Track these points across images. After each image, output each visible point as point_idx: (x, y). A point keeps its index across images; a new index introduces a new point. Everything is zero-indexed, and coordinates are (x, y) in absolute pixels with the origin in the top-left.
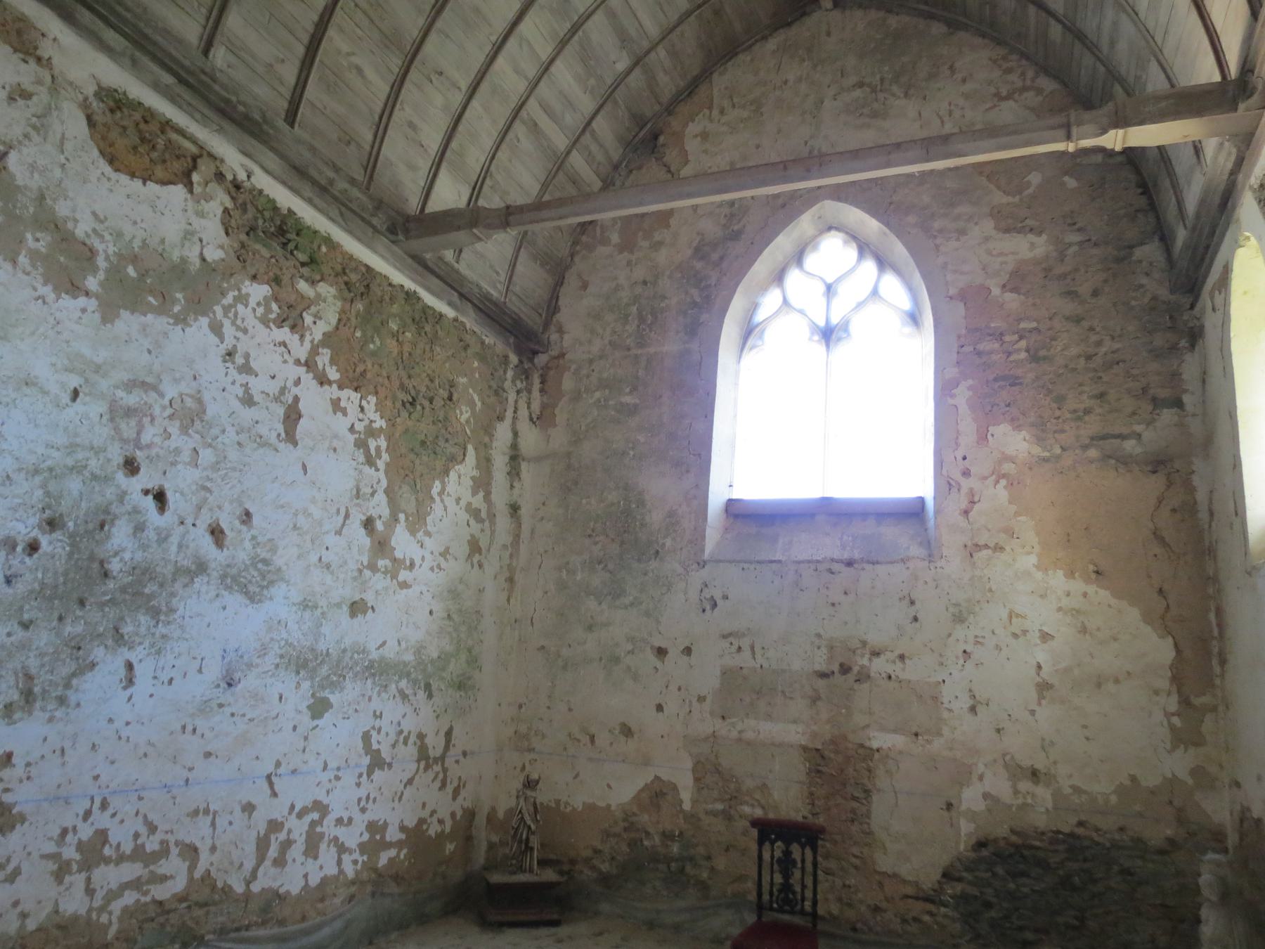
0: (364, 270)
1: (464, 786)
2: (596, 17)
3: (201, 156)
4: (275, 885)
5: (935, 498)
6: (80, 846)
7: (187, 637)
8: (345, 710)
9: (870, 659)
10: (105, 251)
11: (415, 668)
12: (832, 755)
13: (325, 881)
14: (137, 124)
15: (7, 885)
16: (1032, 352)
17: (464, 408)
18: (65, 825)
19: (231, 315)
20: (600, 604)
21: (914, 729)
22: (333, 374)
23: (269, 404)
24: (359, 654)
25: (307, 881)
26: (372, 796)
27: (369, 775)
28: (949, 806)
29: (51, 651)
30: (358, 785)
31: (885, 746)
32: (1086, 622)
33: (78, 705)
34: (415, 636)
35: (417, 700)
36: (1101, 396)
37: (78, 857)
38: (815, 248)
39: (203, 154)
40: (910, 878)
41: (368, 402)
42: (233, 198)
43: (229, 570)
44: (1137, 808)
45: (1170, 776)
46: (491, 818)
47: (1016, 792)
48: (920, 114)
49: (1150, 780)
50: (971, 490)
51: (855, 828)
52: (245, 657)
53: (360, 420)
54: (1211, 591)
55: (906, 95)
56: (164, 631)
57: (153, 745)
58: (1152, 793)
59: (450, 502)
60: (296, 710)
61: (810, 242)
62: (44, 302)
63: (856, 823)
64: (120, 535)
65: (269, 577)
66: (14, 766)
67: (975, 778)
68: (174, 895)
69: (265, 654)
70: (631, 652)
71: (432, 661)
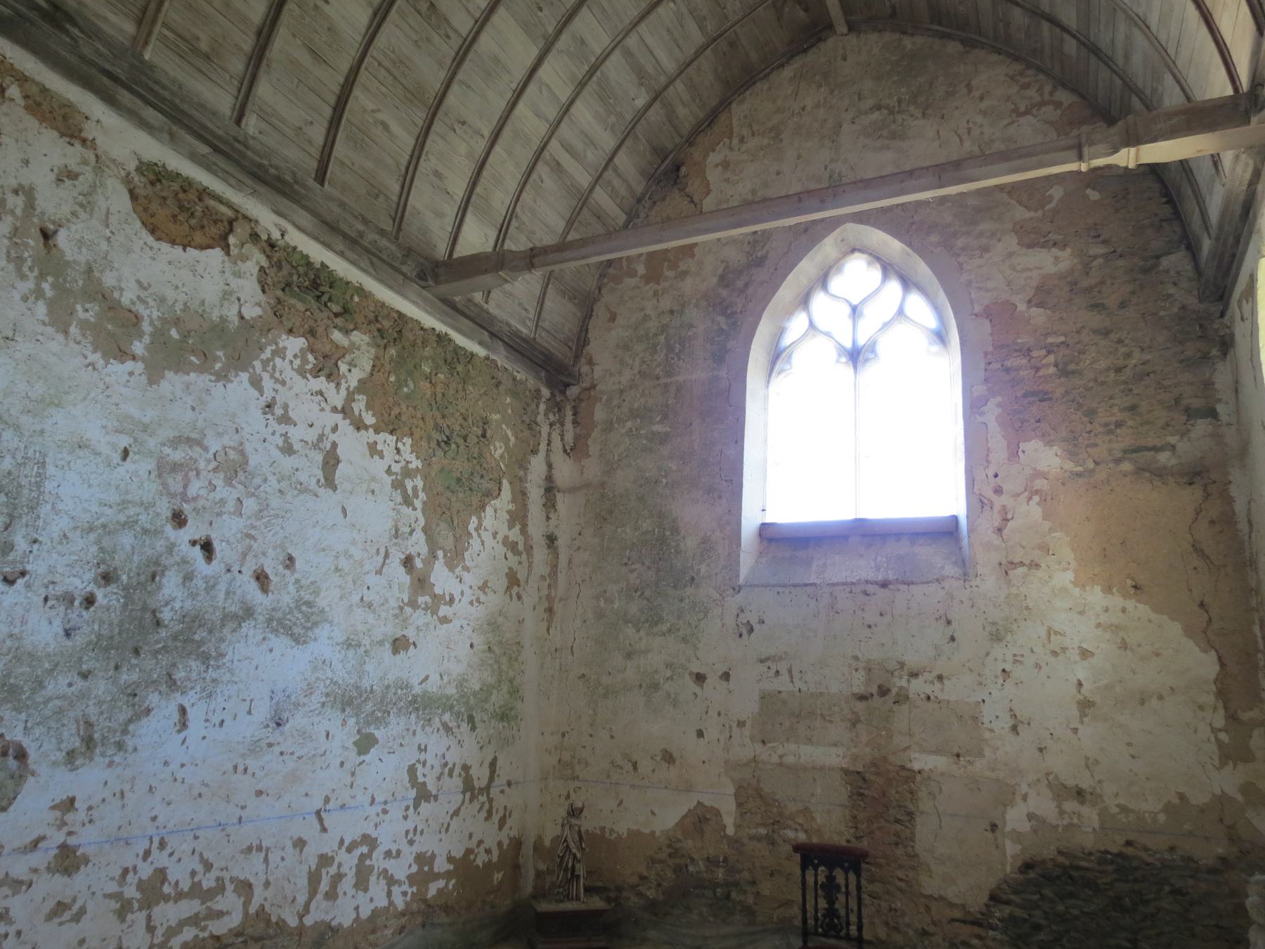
0: (396, 316)
1: (510, 816)
2: (613, 57)
3: (237, 219)
4: (328, 918)
5: (968, 517)
6: (141, 886)
7: (237, 679)
8: (390, 744)
9: (908, 681)
10: (149, 316)
11: (458, 701)
12: (873, 778)
13: (375, 913)
14: (176, 194)
15: (73, 924)
16: (1060, 367)
17: (498, 444)
18: (126, 865)
19: (269, 369)
20: (638, 631)
21: (956, 750)
22: (369, 419)
23: (307, 452)
24: (402, 689)
25: (358, 914)
26: (419, 829)
27: (416, 807)
28: (994, 827)
29: (109, 699)
30: (405, 818)
31: (927, 768)
32: (1126, 638)
33: (135, 749)
34: (457, 669)
35: (461, 733)
36: (1133, 408)
37: (138, 896)
38: (839, 270)
39: (240, 216)
40: (956, 901)
41: (404, 444)
42: (268, 257)
43: (273, 614)
44: (1187, 827)
45: (1218, 792)
46: (538, 846)
47: (1062, 812)
48: (938, 133)
49: (1199, 798)
50: (1004, 507)
51: (900, 851)
52: (293, 697)
53: (396, 462)
54: (1254, 603)
55: (924, 115)
56: (214, 675)
57: (207, 785)
58: (1203, 811)
59: (487, 536)
60: (343, 747)
61: (835, 264)
62: (94, 369)
63: (900, 846)
64: (171, 585)
65: (314, 618)
66: (77, 810)
67: (1018, 799)
68: (230, 930)
69: (311, 693)
70: (671, 678)
71: (475, 694)
